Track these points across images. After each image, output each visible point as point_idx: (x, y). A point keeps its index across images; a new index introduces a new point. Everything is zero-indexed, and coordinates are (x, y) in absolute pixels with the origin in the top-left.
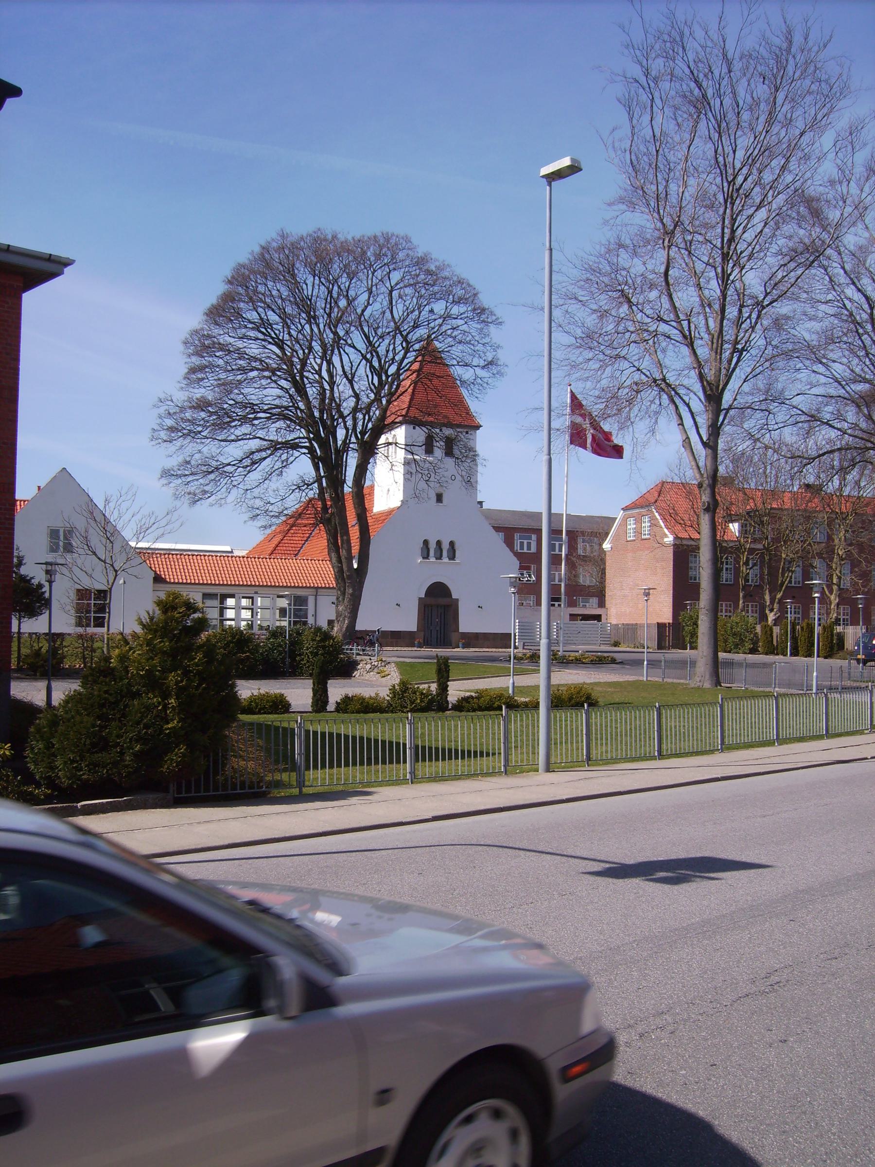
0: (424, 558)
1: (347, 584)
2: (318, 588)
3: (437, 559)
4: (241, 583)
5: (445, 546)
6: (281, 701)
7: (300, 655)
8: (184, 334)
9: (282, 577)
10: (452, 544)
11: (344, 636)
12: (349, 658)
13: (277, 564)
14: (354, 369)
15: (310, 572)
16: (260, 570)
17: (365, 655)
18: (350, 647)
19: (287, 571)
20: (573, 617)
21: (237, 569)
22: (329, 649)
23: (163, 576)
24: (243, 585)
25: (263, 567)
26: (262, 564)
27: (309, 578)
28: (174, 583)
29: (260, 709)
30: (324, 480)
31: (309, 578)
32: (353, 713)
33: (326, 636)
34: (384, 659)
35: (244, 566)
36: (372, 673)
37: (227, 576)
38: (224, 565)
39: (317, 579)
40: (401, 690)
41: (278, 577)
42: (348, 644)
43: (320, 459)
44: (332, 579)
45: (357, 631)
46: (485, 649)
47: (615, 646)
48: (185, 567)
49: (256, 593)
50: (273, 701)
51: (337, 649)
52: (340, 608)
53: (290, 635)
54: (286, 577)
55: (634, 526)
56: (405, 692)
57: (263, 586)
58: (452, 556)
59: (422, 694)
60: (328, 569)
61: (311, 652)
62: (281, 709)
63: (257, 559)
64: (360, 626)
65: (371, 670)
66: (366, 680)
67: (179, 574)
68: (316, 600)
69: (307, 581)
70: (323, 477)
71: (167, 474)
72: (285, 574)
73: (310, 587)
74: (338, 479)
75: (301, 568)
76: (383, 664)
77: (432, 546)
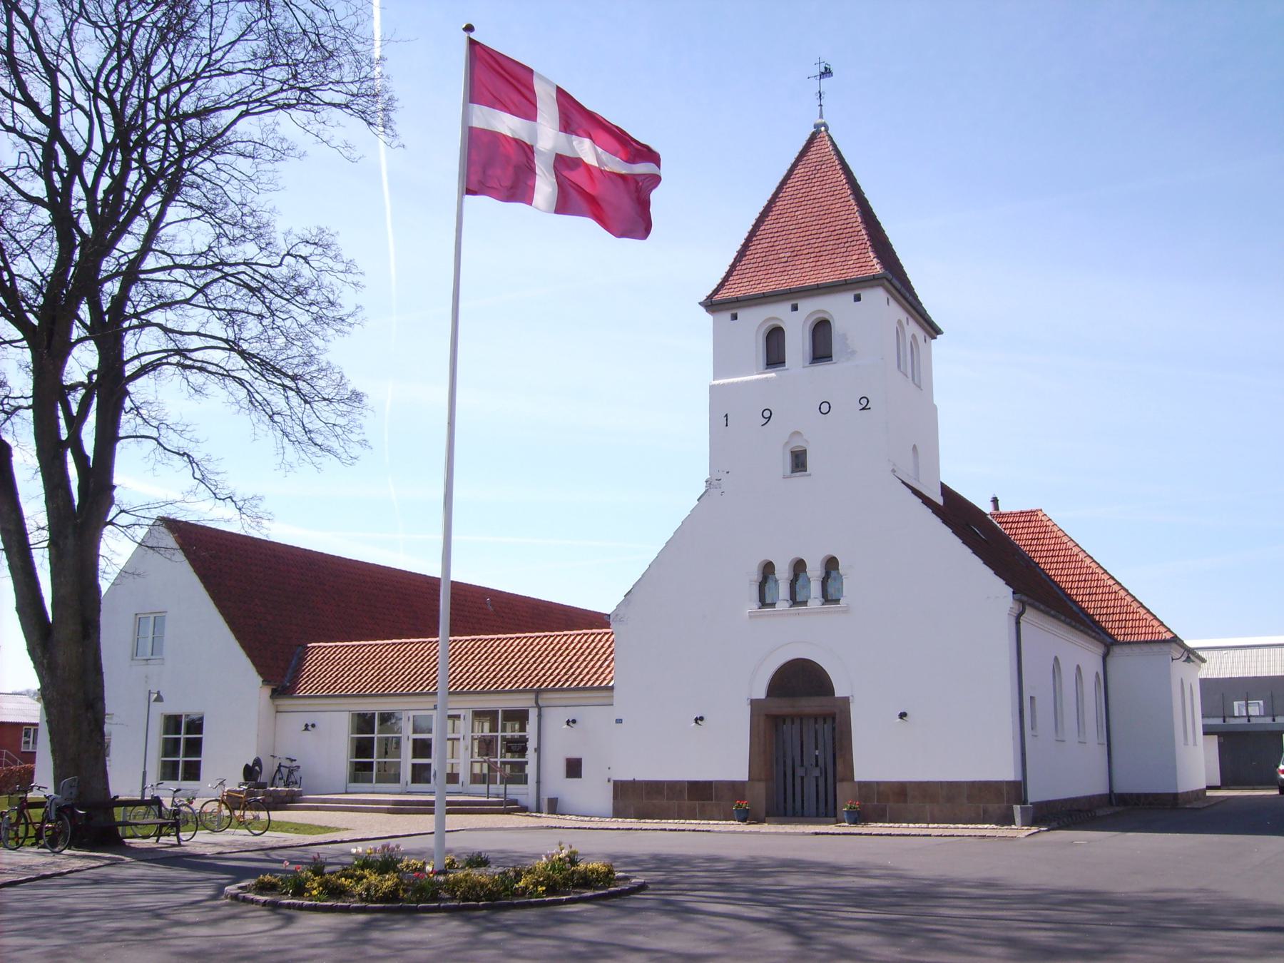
5: (815, 571)
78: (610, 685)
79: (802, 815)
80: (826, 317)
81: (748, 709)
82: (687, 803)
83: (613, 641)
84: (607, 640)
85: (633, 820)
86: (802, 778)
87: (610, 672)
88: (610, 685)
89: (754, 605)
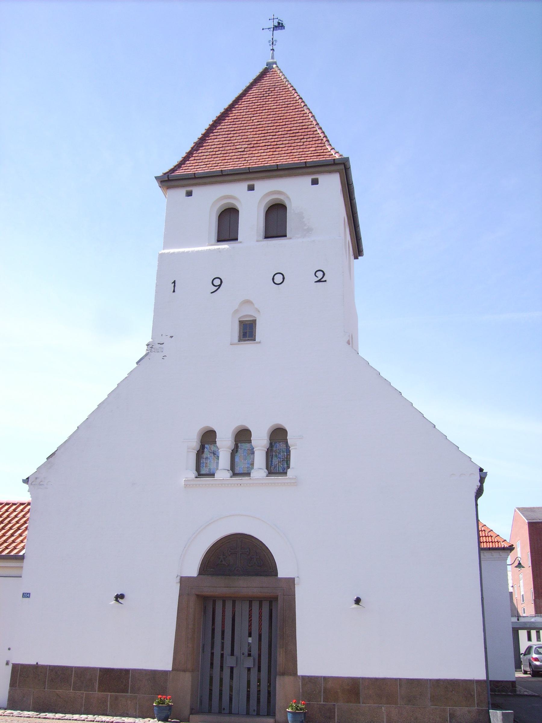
78: (21, 554)
79: (230, 713)
80: (281, 197)
83: (25, 538)
84: (22, 511)
85: (31, 713)
86: (232, 669)
87: (22, 541)
88: (21, 554)
89: (192, 474)
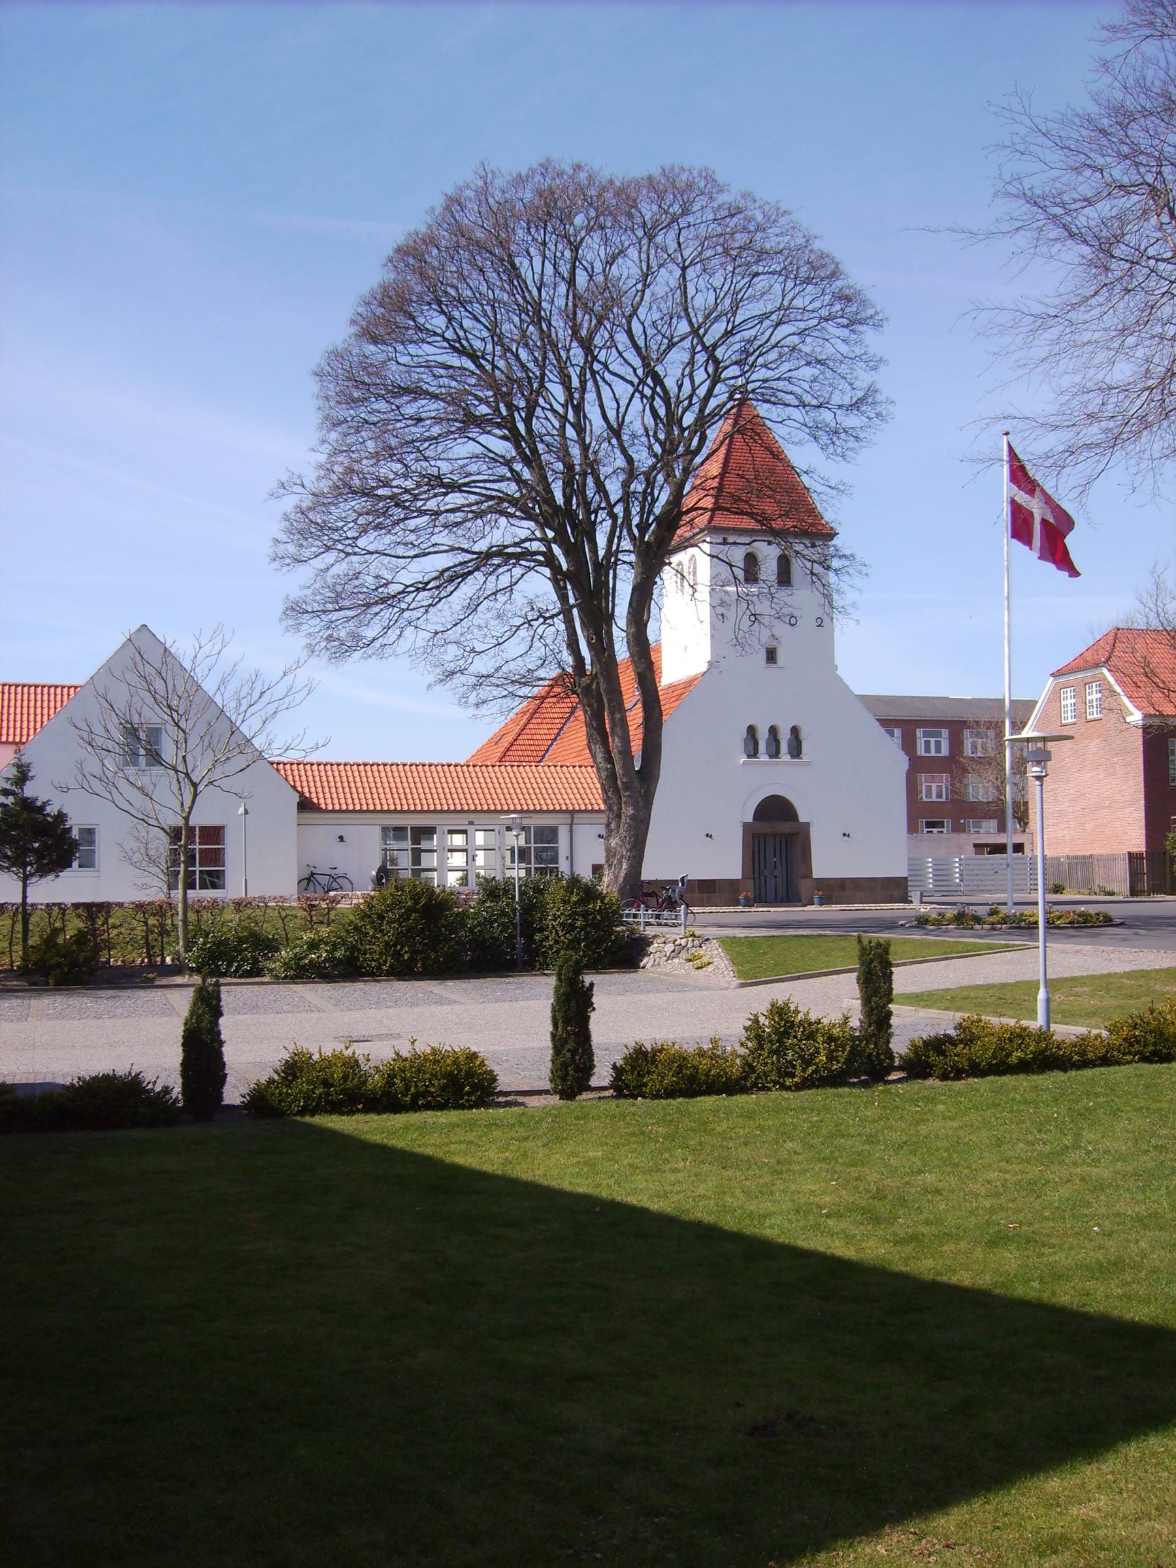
0: (749, 756)
1: (624, 800)
2: (573, 812)
3: (771, 757)
4: (446, 808)
5: (785, 736)
6: (470, 1074)
7: (541, 930)
8: (316, 358)
9: (514, 796)
10: (795, 731)
11: (621, 891)
12: (633, 932)
13: (505, 775)
14: (622, 410)
15: (560, 786)
16: (477, 785)
17: (659, 924)
18: (634, 911)
19: (522, 785)
20: (979, 847)
21: (439, 785)
22: (595, 918)
23: (315, 801)
24: (448, 811)
25: (482, 780)
26: (480, 775)
27: (559, 796)
28: (333, 811)
29: (416, 1097)
30: (575, 611)
31: (559, 796)
32: (657, 1096)
33: (589, 893)
34: (697, 933)
35: (450, 780)
36: (676, 961)
37: (422, 796)
38: (417, 780)
39: (572, 796)
40: (776, 1031)
41: (508, 796)
42: (630, 905)
43: (567, 576)
44: (597, 796)
45: (643, 882)
46: (856, 906)
47: (1056, 892)
48: (352, 785)
49: (471, 823)
50: (449, 1075)
51: (610, 916)
52: (613, 842)
53: (522, 894)
54: (521, 796)
55: (1073, 701)
56: (786, 1034)
57: (482, 811)
58: (796, 750)
59: (831, 1039)
60: (589, 781)
61: (561, 924)
62: (469, 1094)
63: (471, 768)
64: (649, 873)
65: (675, 953)
66: (666, 975)
67: (341, 795)
68: (571, 831)
69: (555, 801)
70: (573, 606)
71: (295, 610)
72: (518, 791)
73: (561, 811)
74: (601, 610)
75: (545, 780)
76: (696, 942)
77: (763, 735)
81: (741, 829)
82: (697, 895)
